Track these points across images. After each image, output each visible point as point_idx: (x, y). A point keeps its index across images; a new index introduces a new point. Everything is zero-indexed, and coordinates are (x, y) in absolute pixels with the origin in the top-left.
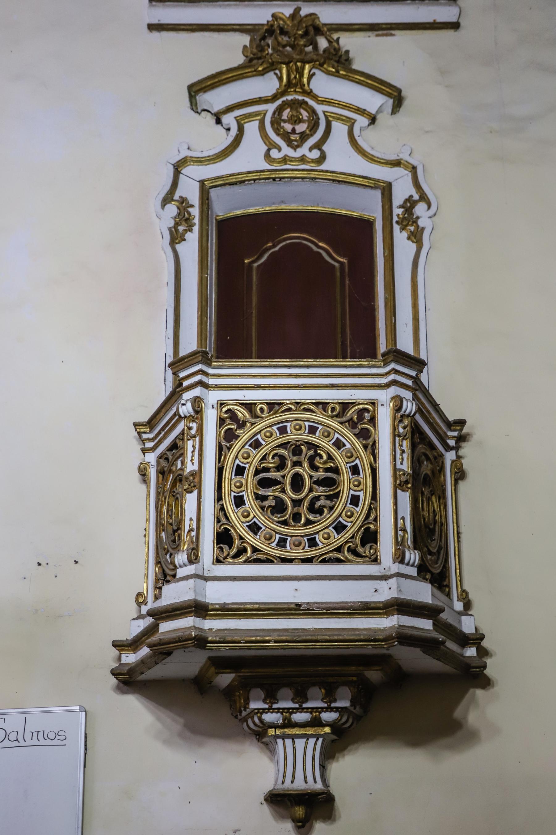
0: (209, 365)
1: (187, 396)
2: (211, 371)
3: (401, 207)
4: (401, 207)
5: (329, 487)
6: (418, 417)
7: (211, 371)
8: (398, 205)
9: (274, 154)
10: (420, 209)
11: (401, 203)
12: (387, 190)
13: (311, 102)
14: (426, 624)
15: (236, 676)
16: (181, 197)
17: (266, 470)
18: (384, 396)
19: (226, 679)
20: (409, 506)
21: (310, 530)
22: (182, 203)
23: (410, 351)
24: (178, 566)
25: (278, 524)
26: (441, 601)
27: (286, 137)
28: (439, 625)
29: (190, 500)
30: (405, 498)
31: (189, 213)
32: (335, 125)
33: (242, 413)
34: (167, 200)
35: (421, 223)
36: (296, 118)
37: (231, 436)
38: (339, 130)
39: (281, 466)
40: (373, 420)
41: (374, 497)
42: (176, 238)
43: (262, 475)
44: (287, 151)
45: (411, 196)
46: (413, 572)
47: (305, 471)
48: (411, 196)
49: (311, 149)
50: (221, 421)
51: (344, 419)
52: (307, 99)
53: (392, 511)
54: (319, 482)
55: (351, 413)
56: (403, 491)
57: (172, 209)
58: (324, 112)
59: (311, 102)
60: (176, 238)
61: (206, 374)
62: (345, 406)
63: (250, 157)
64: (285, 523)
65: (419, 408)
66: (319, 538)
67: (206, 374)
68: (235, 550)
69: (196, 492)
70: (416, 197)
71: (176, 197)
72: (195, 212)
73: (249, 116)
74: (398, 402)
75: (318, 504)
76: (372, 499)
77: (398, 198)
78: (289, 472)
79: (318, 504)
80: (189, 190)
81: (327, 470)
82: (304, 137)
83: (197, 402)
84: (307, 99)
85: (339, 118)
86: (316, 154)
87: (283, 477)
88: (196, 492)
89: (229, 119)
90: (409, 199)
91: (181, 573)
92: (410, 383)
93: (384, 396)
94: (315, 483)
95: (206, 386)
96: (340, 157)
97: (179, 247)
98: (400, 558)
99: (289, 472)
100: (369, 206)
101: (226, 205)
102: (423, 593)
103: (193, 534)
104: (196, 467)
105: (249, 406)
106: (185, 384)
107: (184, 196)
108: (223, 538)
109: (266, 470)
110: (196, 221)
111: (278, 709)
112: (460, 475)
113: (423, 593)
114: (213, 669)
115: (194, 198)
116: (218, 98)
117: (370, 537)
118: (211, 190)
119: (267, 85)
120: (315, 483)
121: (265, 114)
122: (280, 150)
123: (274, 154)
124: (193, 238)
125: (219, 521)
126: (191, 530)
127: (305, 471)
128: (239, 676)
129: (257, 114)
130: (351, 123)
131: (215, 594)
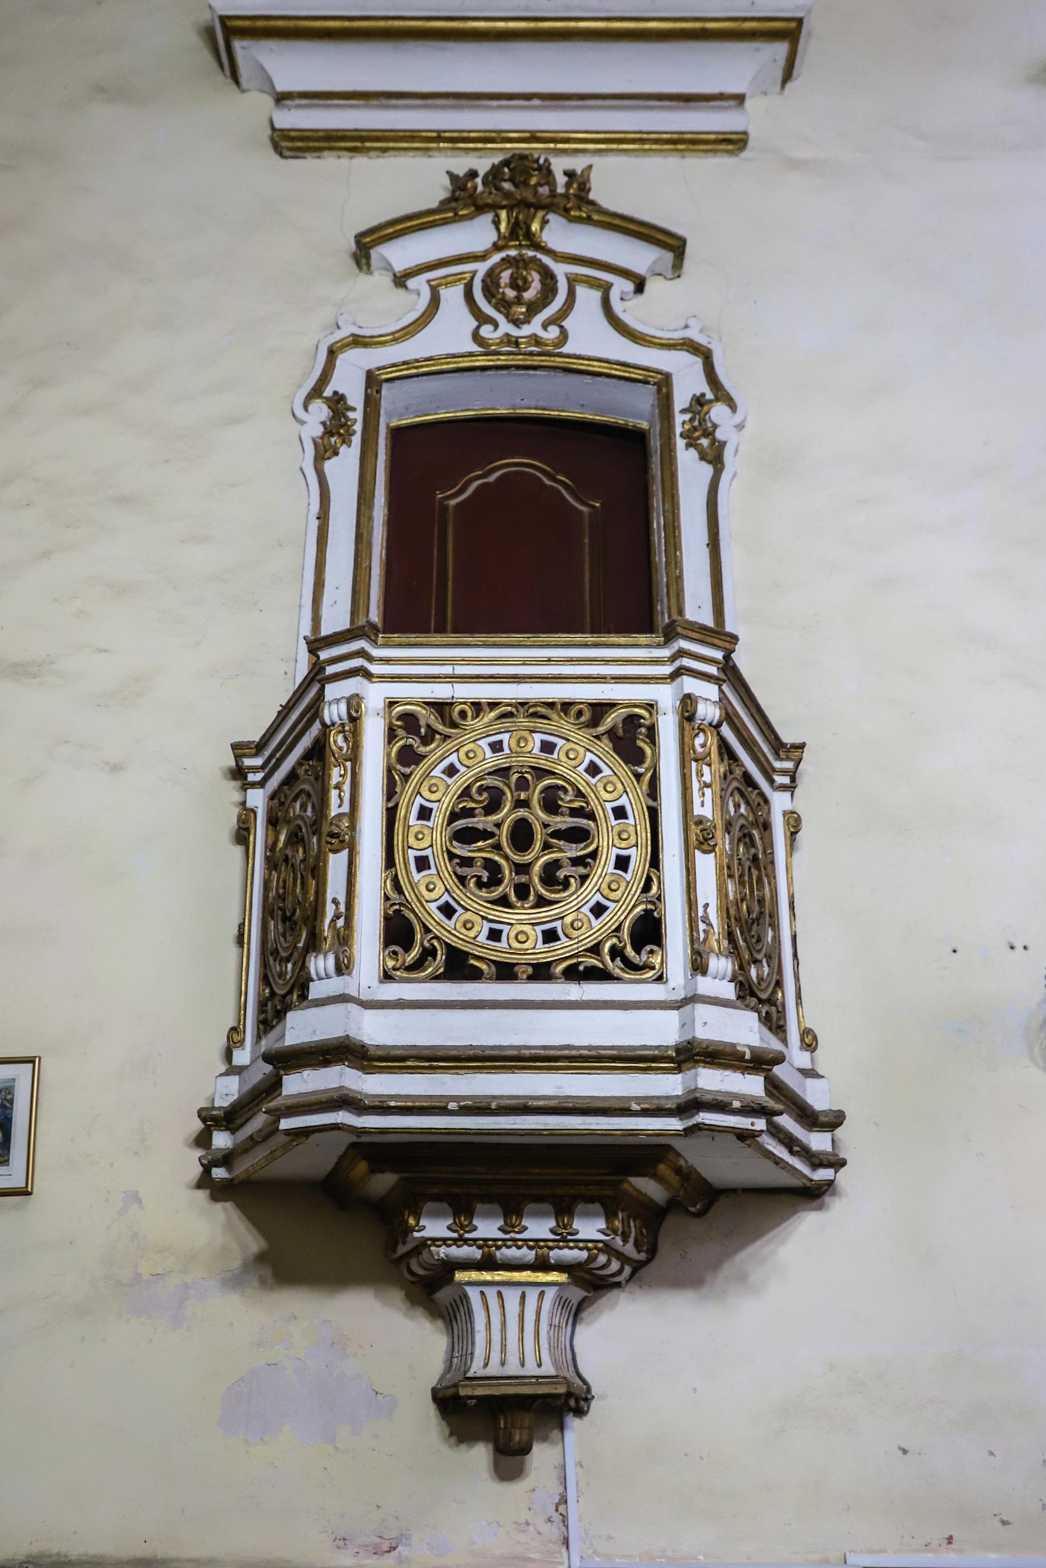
0: (374, 643)
1: (332, 691)
2: (376, 653)
3: (684, 411)
4: (684, 411)
5: (582, 842)
6: (726, 730)
7: (376, 653)
8: (681, 408)
9: (486, 331)
10: (718, 412)
11: (687, 405)
12: (663, 384)
13: (546, 260)
14: (753, 1086)
15: (400, 1179)
16: (335, 393)
17: (468, 813)
18: (665, 696)
19: (384, 1182)
20: (678, 874)
21: (545, 913)
22: (338, 402)
23: (709, 621)
24: (314, 976)
25: (489, 905)
26: (774, 1044)
27: (504, 305)
28: (774, 1086)
29: (336, 864)
30: (706, 865)
31: (347, 419)
32: (581, 291)
33: (427, 717)
34: (316, 392)
35: (719, 435)
36: (518, 284)
37: (409, 757)
38: (588, 298)
39: (493, 807)
40: (652, 733)
41: (655, 862)
42: (324, 452)
43: (460, 824)
44: (506, 327)
45: (703, 395)
46: (729, 991)
47: (537, 815)
48: (703, 395)
49: (545, 326)
50: (391, 735)
51: (601, 729)
52: (539, 256)
53: (694, 887)
54: (486, 835)
55: (610, 720)
56: (705, 852)
57: (320, 411)
58: (566, 275)
59: (546, 260)
60: (324, 452)
61: (370, 659)
62: (600, 709)
63: (452, 333)
64: (503, 902)
65: (727, 714)
66: (460, 915)
67: (370, 659)
68: (415, 953)
69: (346, 852)
70: (710, 396)
71: (328, 392)
72: (357, 416)
73: (448, 281)
74: (687, 706)
75: (561, 874)
76: (651, 866)
77: (681, 399)
78: (507, 815)
79: (561, 874)
80: (348, 381)
81: (575, 812)
82: (534, 308)
83: (354, 703)
84: (539, 256)
85: (593, 283)
86: (553, 332)
87: (498, 825)
88: (346, 852)
89: (419, 283)
90: (699, 401)
91: (317, 990)
92: (713, 670)
93: (665, 696)
94: (492, 835)
95: (368, 675)
96: (588, 335)
97: (328, 466)
98: (698, 966)
99: (507, 815)
100: (635, 409)
101: (401, 407)
102: (743, 1030)
103: (340, 923)
104: (346, 808)
105: (441, 707)
106: (330, 670)
107: (341, 392)
108: (398, 931)
109: (468, 813)
110: (358, 427)
111: (475, 1240)
112: (794, 823)
113: (743, 1030)
114: (363, 1166)
115: (356, 398)
116: (402, 253)
117: (648, 930)
118: (385, 386)
119: (477, 234)
120: (492, 835)
121: (472, 278)
122: (496, 326)
123: (486, 331)
124: (349, 457)
125: (387, 898)
126: (337, 916)
127: (537, 815)
128: (405, 1179)
129: (457, 278)
130: (606, 289)
131: (376, 1030)
